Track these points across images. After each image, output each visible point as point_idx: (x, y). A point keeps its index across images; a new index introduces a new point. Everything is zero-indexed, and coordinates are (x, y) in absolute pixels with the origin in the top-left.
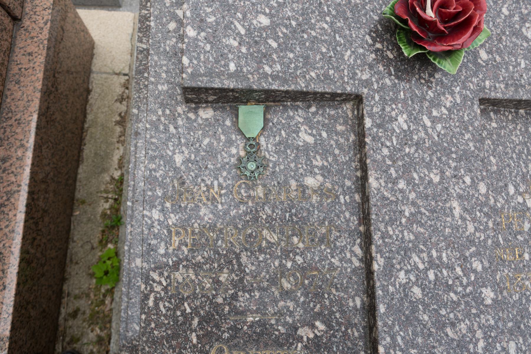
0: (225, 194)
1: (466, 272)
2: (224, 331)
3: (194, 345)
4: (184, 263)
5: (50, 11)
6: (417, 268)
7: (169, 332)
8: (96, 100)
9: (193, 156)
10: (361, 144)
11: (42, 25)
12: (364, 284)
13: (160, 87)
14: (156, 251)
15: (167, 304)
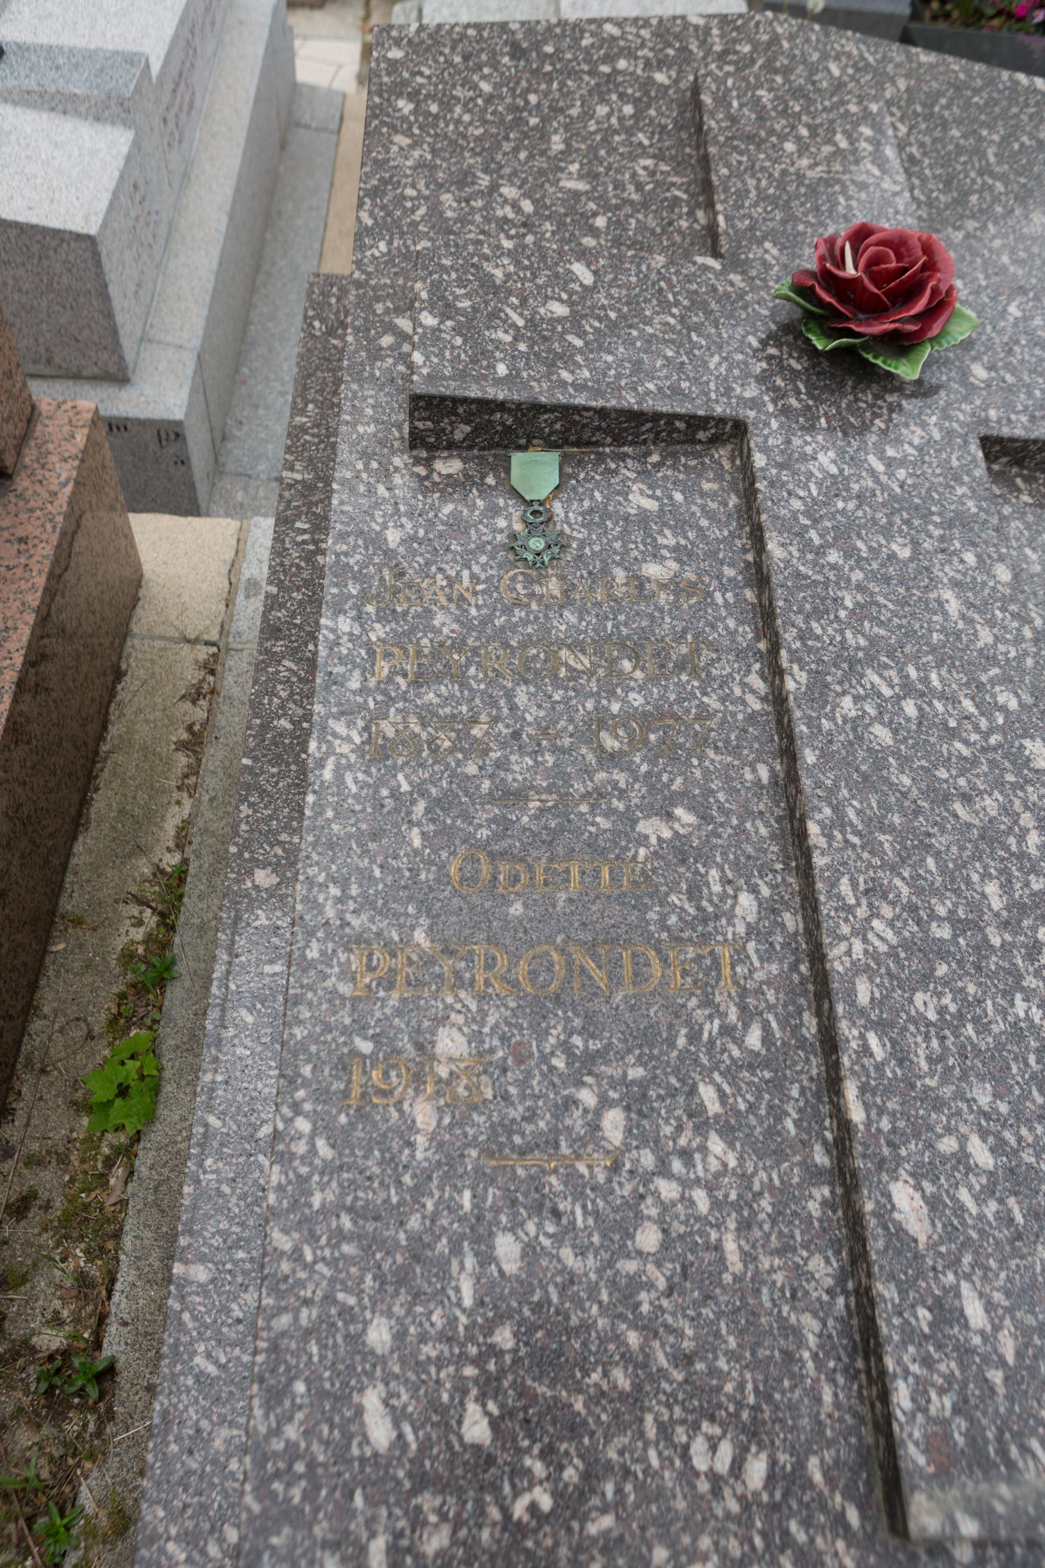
0: (483, 592)
1: (986, 709)
2: (481, 826)
3: (417, 853)
4: (400, 705)
5: (76, 463)
6: (879, 695)
7: (364, 827)
8: (135, 694)
9: (421, 532)
10: (749, 494)
11: (54, 488)
12: (772, 741)
13: (361, 429)
14: (342, 685)
15: (361, 776)
